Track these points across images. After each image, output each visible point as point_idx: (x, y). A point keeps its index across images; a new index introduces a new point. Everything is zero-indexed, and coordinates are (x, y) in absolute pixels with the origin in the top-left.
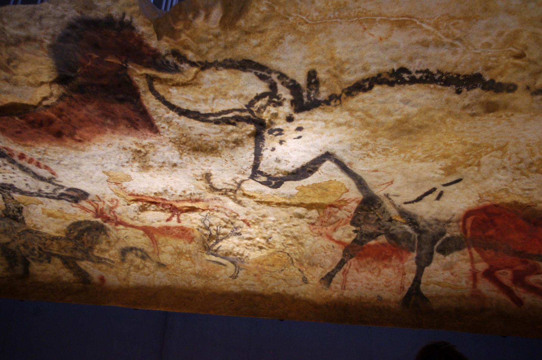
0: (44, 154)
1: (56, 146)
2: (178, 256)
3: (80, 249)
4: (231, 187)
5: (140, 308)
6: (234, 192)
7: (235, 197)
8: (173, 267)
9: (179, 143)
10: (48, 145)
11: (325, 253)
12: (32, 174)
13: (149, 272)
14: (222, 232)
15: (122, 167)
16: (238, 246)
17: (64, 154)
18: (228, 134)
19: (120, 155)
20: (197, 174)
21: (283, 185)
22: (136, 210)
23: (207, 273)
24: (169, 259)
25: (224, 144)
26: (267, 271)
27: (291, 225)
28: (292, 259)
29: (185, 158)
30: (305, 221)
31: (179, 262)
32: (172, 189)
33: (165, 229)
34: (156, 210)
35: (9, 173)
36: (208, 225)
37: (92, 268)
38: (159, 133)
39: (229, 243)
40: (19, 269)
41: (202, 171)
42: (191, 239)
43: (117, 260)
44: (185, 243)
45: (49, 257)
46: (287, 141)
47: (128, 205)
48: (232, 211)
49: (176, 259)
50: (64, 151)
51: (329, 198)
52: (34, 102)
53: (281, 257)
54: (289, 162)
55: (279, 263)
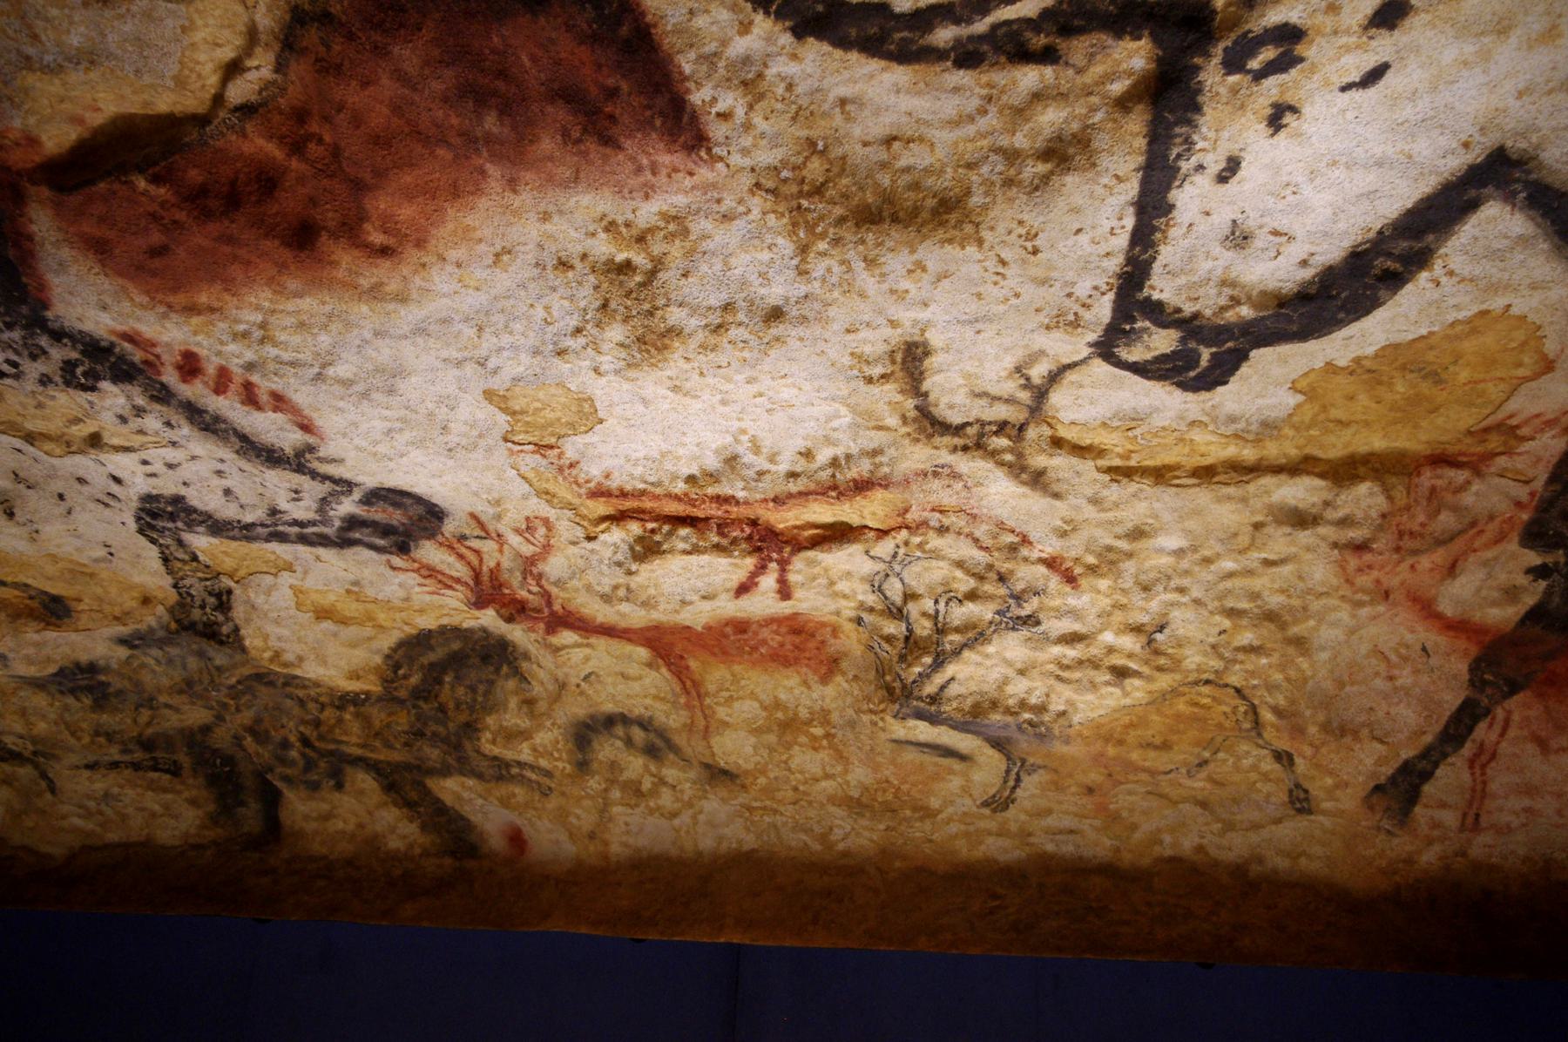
0: (262, 341)
1: (299, 295)
2: (780, 737)
3: (434, 734)
4: (1001, 412)
5: (652, 936)
6: (1014, 432)
7: (1020, 456)
8: (762, 781)
9: (794, 189)
10: (268, 294)
11: (1391, 678)
12: (233, 439)
13: (677, 805)
14: (956, 623)
15: (556, 361)
16: (1022, 672)
17: (335, 327)
18: (1020, 113)
19: (545, 301)
20: (867, 349)
21: (1244, 369)
22: (619, 557)
23: (896, 797)
24: (749, 750)
25: (1000, 168)
26: (1138, 769)
27: (1255, 564)
28: (1254, 710)
29: (818, 267)
30: (1323, 539)
31: (784, 757)
32: (756, 449)
33: (729, 630)
34: (695, 550)
35: (157, 445)
36: (897, 599)
37: (480, 801)
38: (709, 150)
39: (988, 663)
40: (250, 816)
41: (887, 332)
42: (830, 666)
43: (560, 765)
44: (805, 683)
45: (337, 768)
46: (1307, 110)
47: (590, 539)
48: (1001, 525)
49: (771, 750)
50: (330, 316)
51: (1440, 421)
52: (192, 102)
53: (1203, 707)
54: (1291, 239)
55: (1193, 734)
